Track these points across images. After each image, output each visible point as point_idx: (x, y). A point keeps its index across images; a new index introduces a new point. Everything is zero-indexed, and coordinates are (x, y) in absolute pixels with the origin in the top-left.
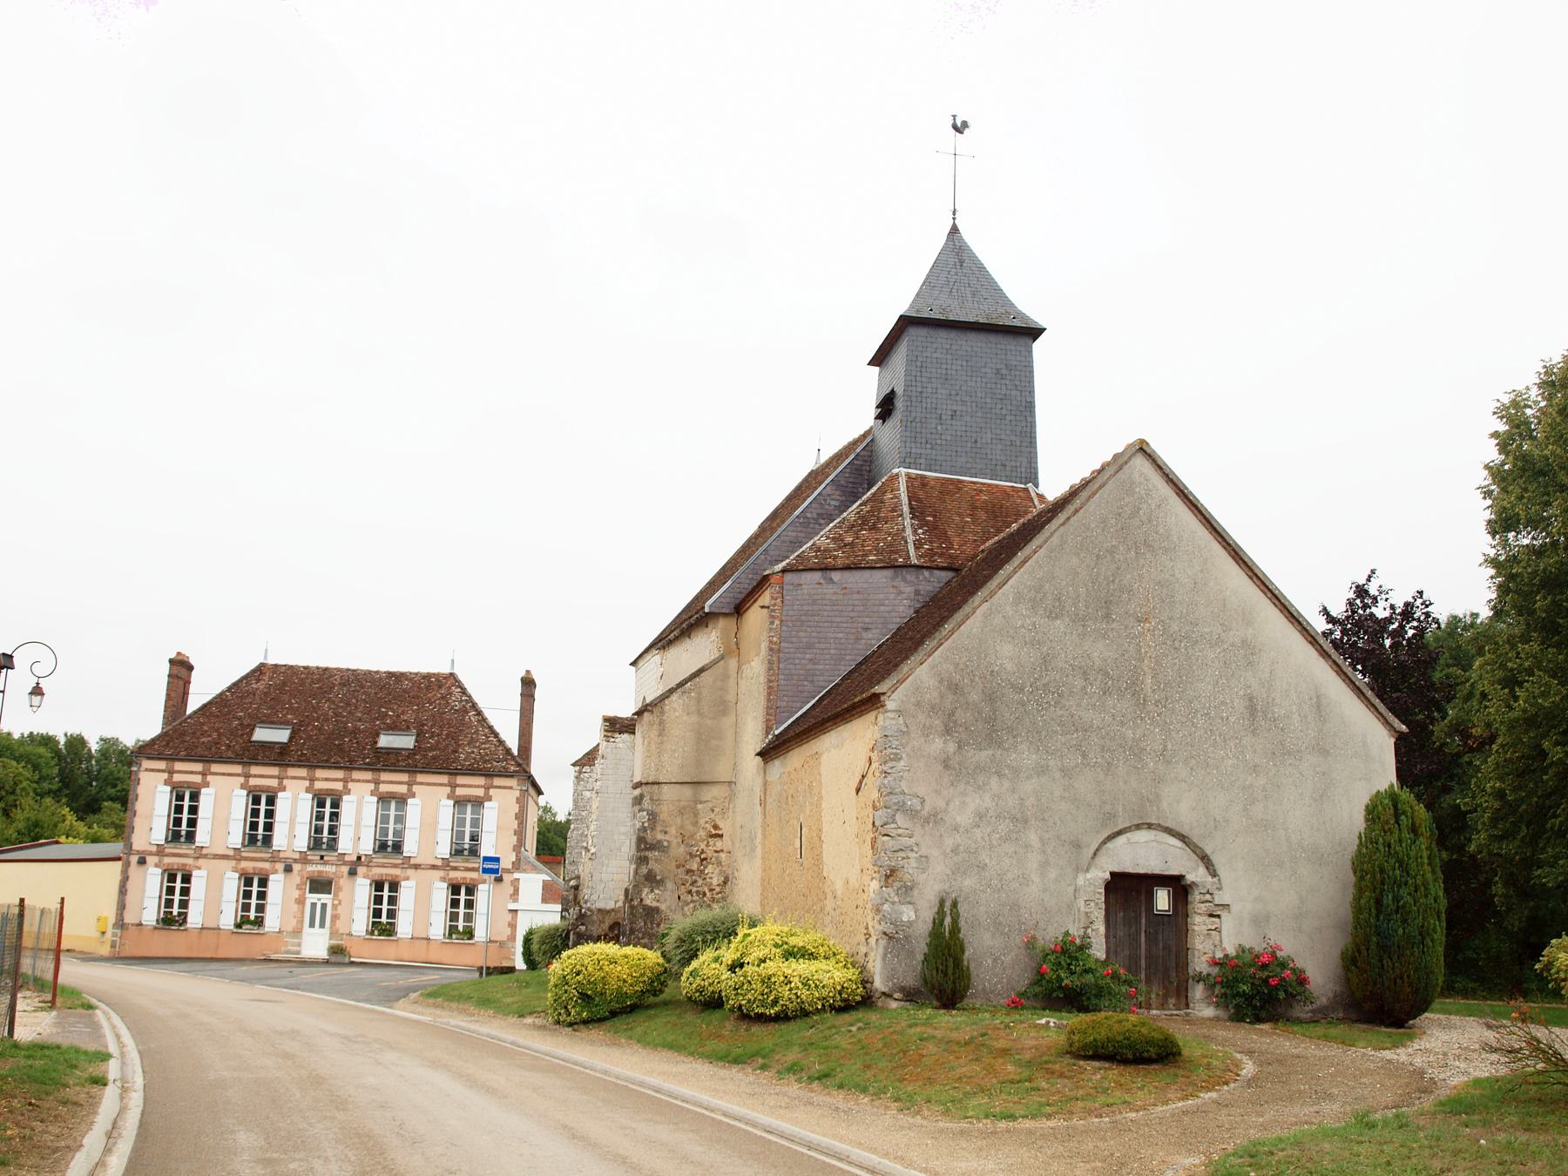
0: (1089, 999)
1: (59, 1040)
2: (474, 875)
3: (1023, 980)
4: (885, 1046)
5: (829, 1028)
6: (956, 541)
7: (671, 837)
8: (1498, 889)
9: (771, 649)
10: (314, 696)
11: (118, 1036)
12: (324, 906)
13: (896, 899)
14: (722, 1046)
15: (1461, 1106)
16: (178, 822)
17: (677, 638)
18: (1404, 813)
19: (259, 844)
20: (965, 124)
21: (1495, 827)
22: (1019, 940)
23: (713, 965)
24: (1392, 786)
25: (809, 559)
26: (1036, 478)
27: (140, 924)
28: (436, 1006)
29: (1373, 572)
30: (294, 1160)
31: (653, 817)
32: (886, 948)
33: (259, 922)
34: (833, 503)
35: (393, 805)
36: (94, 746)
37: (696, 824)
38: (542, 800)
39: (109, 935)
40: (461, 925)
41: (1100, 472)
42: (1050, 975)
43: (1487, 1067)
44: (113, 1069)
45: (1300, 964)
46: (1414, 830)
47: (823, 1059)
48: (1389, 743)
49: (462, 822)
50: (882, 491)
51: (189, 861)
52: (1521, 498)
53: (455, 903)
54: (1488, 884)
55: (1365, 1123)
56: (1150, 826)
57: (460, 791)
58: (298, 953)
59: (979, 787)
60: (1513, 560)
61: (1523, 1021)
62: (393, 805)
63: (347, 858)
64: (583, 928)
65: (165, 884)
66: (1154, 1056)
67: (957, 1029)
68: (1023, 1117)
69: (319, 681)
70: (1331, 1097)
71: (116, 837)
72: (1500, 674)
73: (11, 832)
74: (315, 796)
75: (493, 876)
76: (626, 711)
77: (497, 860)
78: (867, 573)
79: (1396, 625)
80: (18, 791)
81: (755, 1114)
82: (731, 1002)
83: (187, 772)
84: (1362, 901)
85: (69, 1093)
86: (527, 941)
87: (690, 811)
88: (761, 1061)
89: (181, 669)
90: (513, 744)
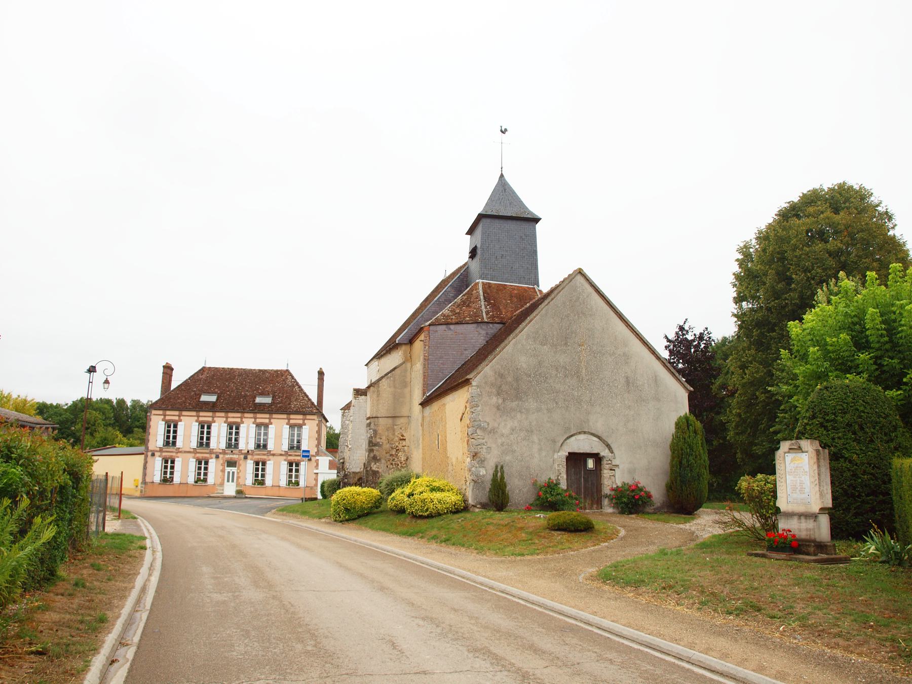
0: (559, 506)
1: (124, 532)
2: (299, 458)
3: (532, 500)
4: (472, 527)
5: (450, 520)
6: (504, 311)
7: (383, 440)
8: (739, 455)
9: (425, 359)
10: (227, 381)
11: (148, 530)
12: (233, 473)
13: (478, 466)
14: (405, 529)
15: (706, 546)
16: (168, 437)
17: (384, 354)
18: (691, 425)
19: (204, 446)
20: (506, 130)
21: (737, 429)
22: (529, 482)
23: (401, 495)
24: (686, 414)
25: (440, 320)
26: (538, 283)
27: (153, 482)
28: (283, 515)
29: (686, 320)
30: (226, 577)
31: (375, 432)
32: (473, 486)
33: (205, 480)
34: (451, 295)
35: (263, 428)
36: (129, 404)
37: (394, 434)
38: (328, 424)
39: (139, 487)
40: (293, 480)
41: (563, 282)
42: (543, 496)
43: (718, 531)
44: (148, 543)
45: (648, 489)
46: (695, 432)
47: (447, 533)
48: (685, 396)
49: (293, 435)
50: (472, 290)
51: (174, 454)
52: (747, 288)
53: (291, 470)
54: (736, 453)
55: (663, 553)
56: (585, 433)
57: (292, 422)
58: (222, 493)
59: (512, 418)
60: (744, 314)
61: (731, 510)
62: (263, 428)
63: (243, 452)
64: (346, 480)
65: (164, 464)
66: (583, 529)
67: (502, 520)
68: (527, 555)
69: (229, 374)
70: (654, 543)
71: (141, 444)
72: (739, 363)
73: (94, 443)
74: (228, 425)
75: (307, 459)
76: (363, 386)
77: (308, 451)
78: (465, 326)
79: (697, 342)
80: (96, 425)
81: (417, 556)
82: (409, 510)
83: (172, 415)
84: (674, 463)
85: (131, 553)
86: (322, 486)
87: (392, 429)
88: (421, 535)
89: (168, 370)
90: (315, 400)
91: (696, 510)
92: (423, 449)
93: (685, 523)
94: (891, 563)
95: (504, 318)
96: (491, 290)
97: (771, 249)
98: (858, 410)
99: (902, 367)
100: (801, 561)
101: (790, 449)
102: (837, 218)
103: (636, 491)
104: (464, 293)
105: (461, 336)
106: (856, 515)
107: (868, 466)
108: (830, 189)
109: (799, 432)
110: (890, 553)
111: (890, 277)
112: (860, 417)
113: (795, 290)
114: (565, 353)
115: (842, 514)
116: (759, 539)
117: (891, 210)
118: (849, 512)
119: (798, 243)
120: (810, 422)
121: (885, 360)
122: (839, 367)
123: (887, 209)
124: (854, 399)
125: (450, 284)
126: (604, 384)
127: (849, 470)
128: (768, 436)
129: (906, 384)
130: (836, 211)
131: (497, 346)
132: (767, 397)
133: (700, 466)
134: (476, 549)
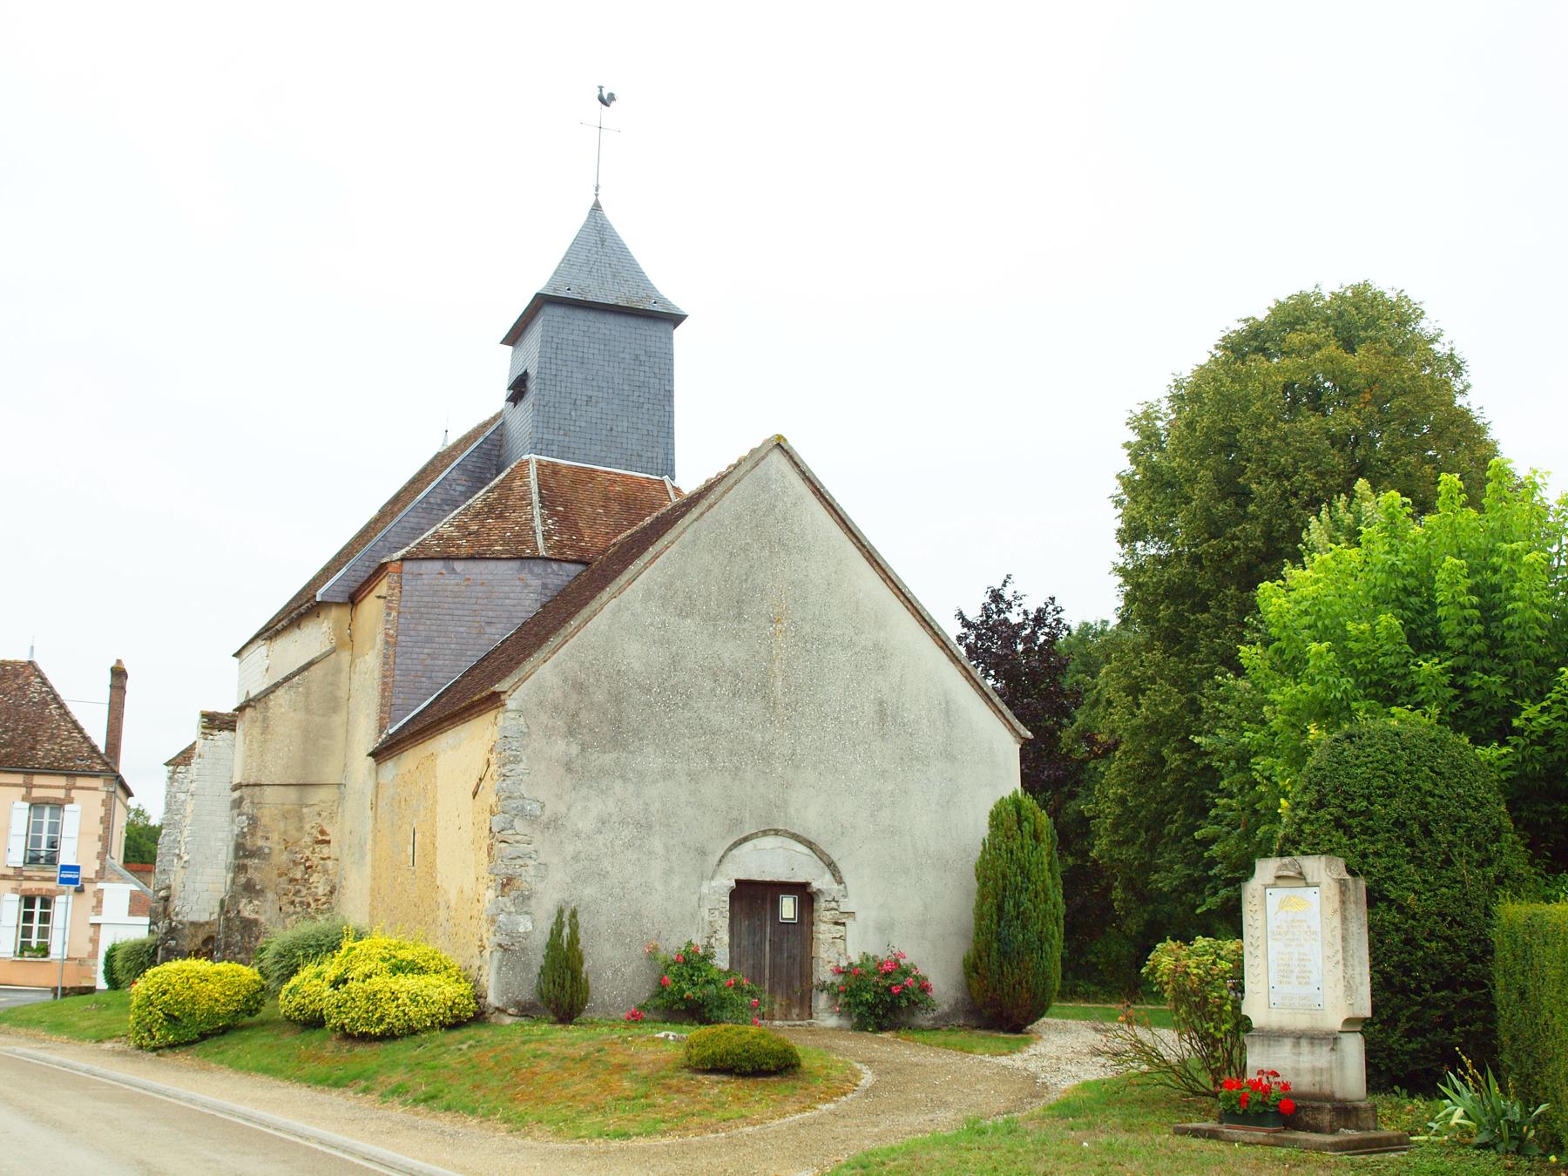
0: (710, 1010)
4: (497, 1064)
5: (439, 1047)
6: (587, 532)
7: (272, 843)
8: (1117, 894)
9: (387, 643)
13: (513, 909)
14: (323, 1069)
15: (1069, 1110)
17: (285, 628)
18: (1026, 819)
20: (612, 97)
21: (1116, 832)
22: (640, 951)
25: (430, 547)
26: (673, 470)
31: (253, 821)
32: (501, 961)
34: (459, 488)
37: (300, 829)
38: (132, 803)
41: (736, 467)
42: (672, 987)
43: (1096, 1071)
45: (923, 971)
46: (1036, 836)
48: (1014, 750)
49: (38, 827)
50: (511, 478)
52: (1149, 508)
53: (28, 917)
54: (1109, 889)
56: (777, 832)
57: (36, 793)
59: (602, 792)
60: (1140, 569)
61: (1129, 1024)
64: (173, 943)
66: (773, 1068)
67: (573, 1045)
70: (945, 1105)
72: (1124, 682)
75: (73, 887)
76: (226, 705)
77: (77, 869)
78: (492, 565)
79: (1029, 630)
81: (354, 1141)
86: (110, 958)
87: (295, 815)
88: (363, 1083)
90: (100, 741)
91: (1032, 1022)
92: (373, 867)
93: (1011, 1052)
94: (1501, 1147)
95: (587, 550)
96: (557, 481)
97: (1206, 422)
98: (1418, 789)
99: (1510, 693)
100: (1306, 1147)
101: (1279, 878)
102: (1351, 361)
103: (895, 975)
104: (492, 484)
105: (479, 588)
106: (1410, 1034)
107: (1439, 919)
108: (1335, 296)
109: (1286, 839)
110: (1497, 1124)
111: (1489, 487)
112: (1424, 805)
113: (1255, 517)
114: (736, 637)
115: (1380, 1031)
116: (1195, 1093)
117: (1461, 353)
118: (1394, 1028)
119: (1266, 411)
120: (1312, 817)
121: (1474, 677)
122: (1372, 691)
123: (1452, 349)
124: (1410, 765)
125: (457, 462)
126: (827, 715)
127: (1398, 930)
128: (1185, 851)
129: (1519, 732)
130: (1349, 346)
131: (570, 615)
132: (1185, 761)
133: (1044, 917)
134: (507, 1121)
